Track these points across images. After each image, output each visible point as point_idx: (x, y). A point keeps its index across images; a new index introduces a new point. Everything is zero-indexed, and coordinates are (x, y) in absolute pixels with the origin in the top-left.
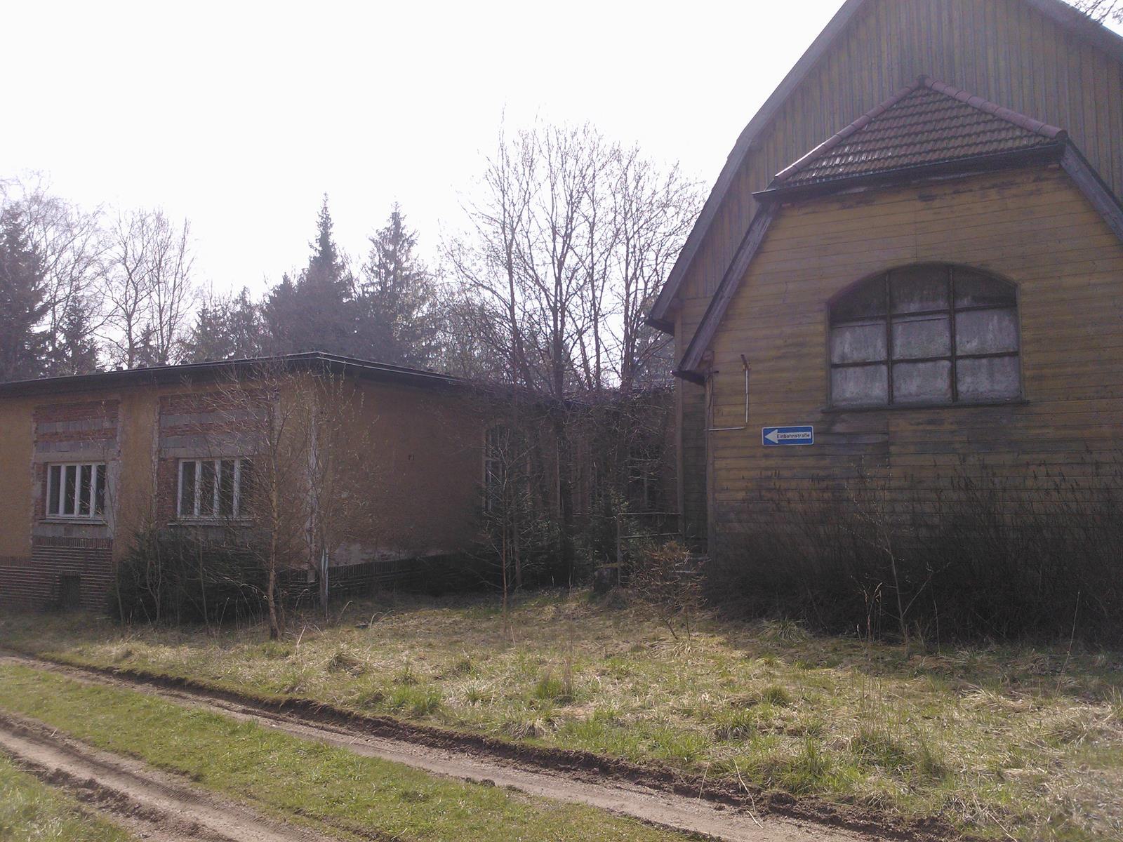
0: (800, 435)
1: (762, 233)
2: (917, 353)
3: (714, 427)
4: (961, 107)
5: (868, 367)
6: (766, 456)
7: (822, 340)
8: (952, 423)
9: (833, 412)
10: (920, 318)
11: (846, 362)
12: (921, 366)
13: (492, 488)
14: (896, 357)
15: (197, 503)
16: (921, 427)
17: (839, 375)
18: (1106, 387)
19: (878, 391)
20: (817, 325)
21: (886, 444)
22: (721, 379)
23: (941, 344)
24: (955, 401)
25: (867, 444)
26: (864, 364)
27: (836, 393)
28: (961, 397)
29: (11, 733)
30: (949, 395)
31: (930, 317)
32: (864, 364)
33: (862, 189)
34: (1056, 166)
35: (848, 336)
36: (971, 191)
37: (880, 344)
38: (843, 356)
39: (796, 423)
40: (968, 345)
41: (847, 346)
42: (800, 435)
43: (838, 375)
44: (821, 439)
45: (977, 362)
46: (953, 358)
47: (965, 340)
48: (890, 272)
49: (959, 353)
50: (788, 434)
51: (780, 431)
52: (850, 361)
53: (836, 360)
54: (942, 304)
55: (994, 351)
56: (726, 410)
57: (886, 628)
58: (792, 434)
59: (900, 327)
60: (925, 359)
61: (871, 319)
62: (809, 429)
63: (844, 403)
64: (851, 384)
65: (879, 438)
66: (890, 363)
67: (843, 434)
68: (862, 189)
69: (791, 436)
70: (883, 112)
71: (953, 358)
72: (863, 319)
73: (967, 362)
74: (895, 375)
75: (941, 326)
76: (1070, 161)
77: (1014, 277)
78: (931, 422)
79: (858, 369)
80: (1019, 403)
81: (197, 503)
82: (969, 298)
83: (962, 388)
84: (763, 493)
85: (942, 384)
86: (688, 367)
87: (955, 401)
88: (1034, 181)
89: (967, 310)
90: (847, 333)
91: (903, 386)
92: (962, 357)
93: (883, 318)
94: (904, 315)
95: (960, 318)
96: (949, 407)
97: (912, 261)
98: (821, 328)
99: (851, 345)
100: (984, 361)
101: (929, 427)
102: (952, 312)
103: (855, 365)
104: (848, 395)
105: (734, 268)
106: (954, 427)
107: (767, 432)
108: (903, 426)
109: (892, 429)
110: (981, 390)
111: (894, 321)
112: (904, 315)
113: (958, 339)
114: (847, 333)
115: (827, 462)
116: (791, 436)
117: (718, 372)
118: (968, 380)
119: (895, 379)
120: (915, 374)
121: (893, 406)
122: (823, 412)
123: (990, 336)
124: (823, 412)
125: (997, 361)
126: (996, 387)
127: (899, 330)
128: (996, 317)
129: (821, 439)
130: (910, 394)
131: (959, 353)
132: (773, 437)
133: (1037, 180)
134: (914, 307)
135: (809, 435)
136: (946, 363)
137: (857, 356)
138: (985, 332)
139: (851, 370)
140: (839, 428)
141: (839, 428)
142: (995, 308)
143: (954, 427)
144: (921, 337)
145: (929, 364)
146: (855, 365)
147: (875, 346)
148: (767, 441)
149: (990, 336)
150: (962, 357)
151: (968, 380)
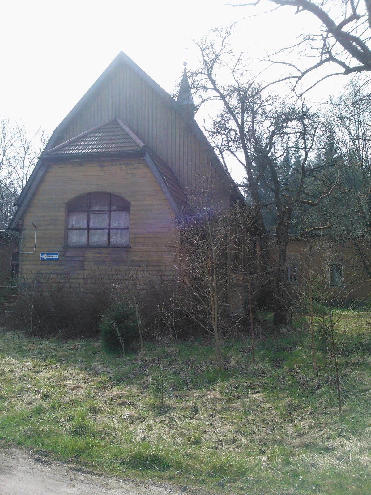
0: (54, 257)
1: (42, 174)
2: (98, 226)
3: (23, 252)
4: (122, 131)
5: (81, 231)
6: (41, 264)
7: (63, 218)
8: (106, 254)
9: (66, 247)
10: (99, 213)
11: (73, 228)
12: (99, 231)
13: (244, 253)
14: (90, 227)
15: (15, 266)
16: (95, 255)
17: (70, 233)
18: (155, 242)
19: (83, 240)
20: (62, 213)
21: (83, 261)
22: (26, 232)
23: (105, 224)
24: (109, 245)
25: (77, 261)
26: (79, 229)
27: (69, 240)
28: (111, 244)
29: (98, 344)
30: (107, 243)
31: (103, 212)
32: (79, 229)
33: (78, 160)
34: (143, 158)
35: (74, 218)
36: (116, 165)
37: (85, 222)
38: (72, 226)
39: (53, 251)
40: (114, 224)
41: (74, 222)
42: (54, 257)
43: (70, 233)
44: (61, 258)
45: (117, 231)
46: (109, 229)
47: (113, 222)
48: (89, 194)
49: (111, 227)
50: (49, 256)
51: (47, 254)
52: (75, 228)
53: (70, 227)
54: (106, 208)
55: (122, 227)
56: (27, 245)
57: (70, 335)
58: (51, 256)
59: (92, 216)
60: (97, 229)
61: (83, 211)
62: (57, 254)
63: (72, 244)
64: (75, 237)
65: (80, 259)
66: (88, 229)
67: (68, 257)
68: (78, 160)
69: (51, 256)
70: (97, 130)
71: (109, 229)
72: (79, 211)
73: (114, 230)
74: (90, 234)
75: (106, 216)
76: (147, 157)
77: (129, 199)
78: (99, 253)
79: (77, 231)
80: (127, 248)
81: (15, 266)
82: (116, 206)
83: (112, 240)
84: (39, 279)
85: (105, 238)
86: (12, 227)
87: (109, 245)
88: (138, 163)
89: (115, 210)
90: (74, 217)
91: (92, 239)
92: (112, 229)
93: (87, 211)
94: (94, 211)
95: (112, 213)
96: (107, 248)
97: (96, 190)
98: (63, 214)
99: (75, 221)
100: (119, 230)
101: (98, 255)
102: (110, 211)
103: (77, 229)
104: (73, 241)
105: (31, 187)
106: (107, 255)
107: (42, 255)
108: (89, 254)
109: (86, 255)
110: (118, 241)
111: (91, 213)
112: (94, 211)
113: (111, 221)
114: (74, 217)
115: (62, 268)
116: (51, 256)
117: (25, 229)
118: (114, 237)
119: (90, 236)
120: (96, 234)
121: (88, 246)
122: (62, 247)
123: (122, 221)
124: (62, 247)
125: (123, 231)
126: (123, 241)
127: (92, 217)
128: (124, 214)
129: (61, 258)
130: (94, 242)
131: (111, 227)
132: (44, 257)
133: (138, 163)
134: (97, 208)
135: (57, 257)
136: (107, 230)
137: (77, 226)
138: (120, 220)
139: (75, 231)
140: (68, 254)
141: (68, 254)
142: (124, 211)
143: (107, 255)
144: (99, 221)
145: (101, 231)
146: (77, 229)
147: (83, 223)
148: (42, 258)
149: (122, 221)
150: (112, 229)
151: (114, 237)
